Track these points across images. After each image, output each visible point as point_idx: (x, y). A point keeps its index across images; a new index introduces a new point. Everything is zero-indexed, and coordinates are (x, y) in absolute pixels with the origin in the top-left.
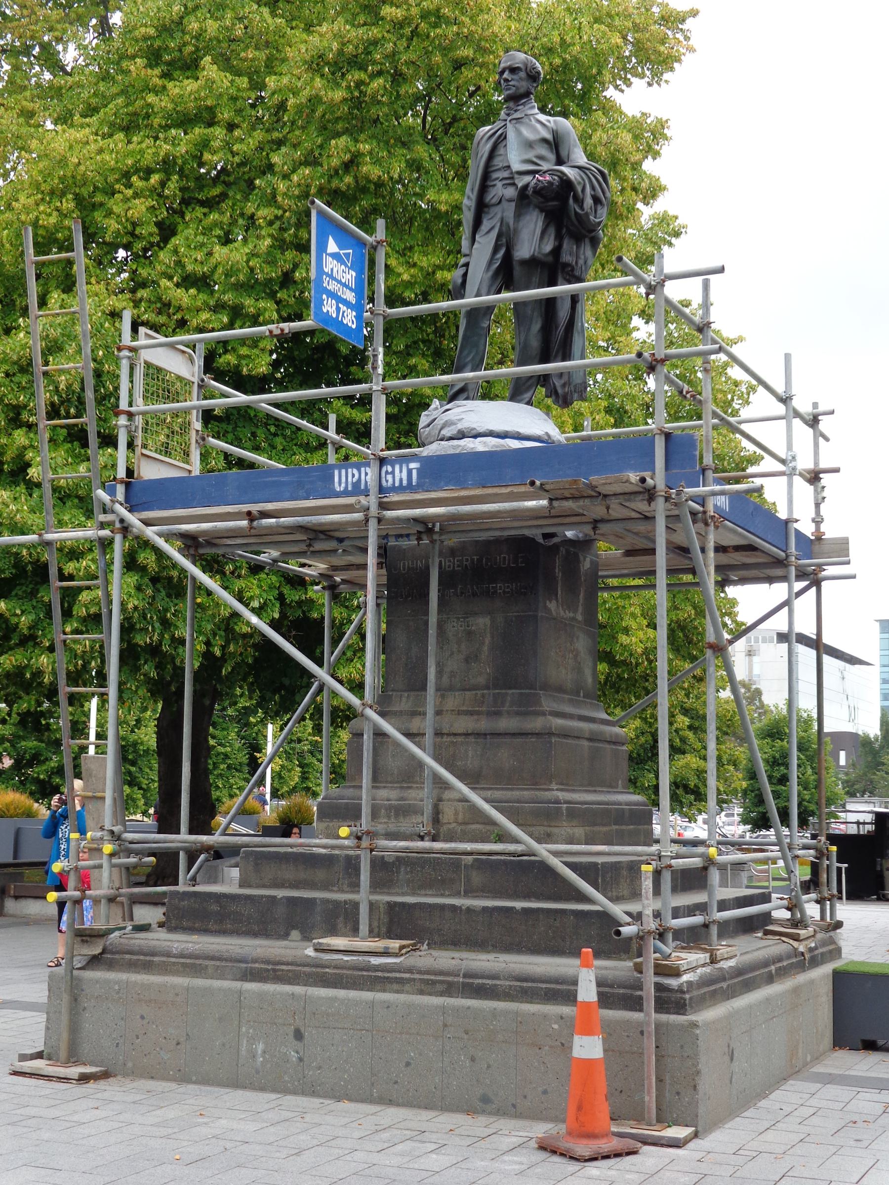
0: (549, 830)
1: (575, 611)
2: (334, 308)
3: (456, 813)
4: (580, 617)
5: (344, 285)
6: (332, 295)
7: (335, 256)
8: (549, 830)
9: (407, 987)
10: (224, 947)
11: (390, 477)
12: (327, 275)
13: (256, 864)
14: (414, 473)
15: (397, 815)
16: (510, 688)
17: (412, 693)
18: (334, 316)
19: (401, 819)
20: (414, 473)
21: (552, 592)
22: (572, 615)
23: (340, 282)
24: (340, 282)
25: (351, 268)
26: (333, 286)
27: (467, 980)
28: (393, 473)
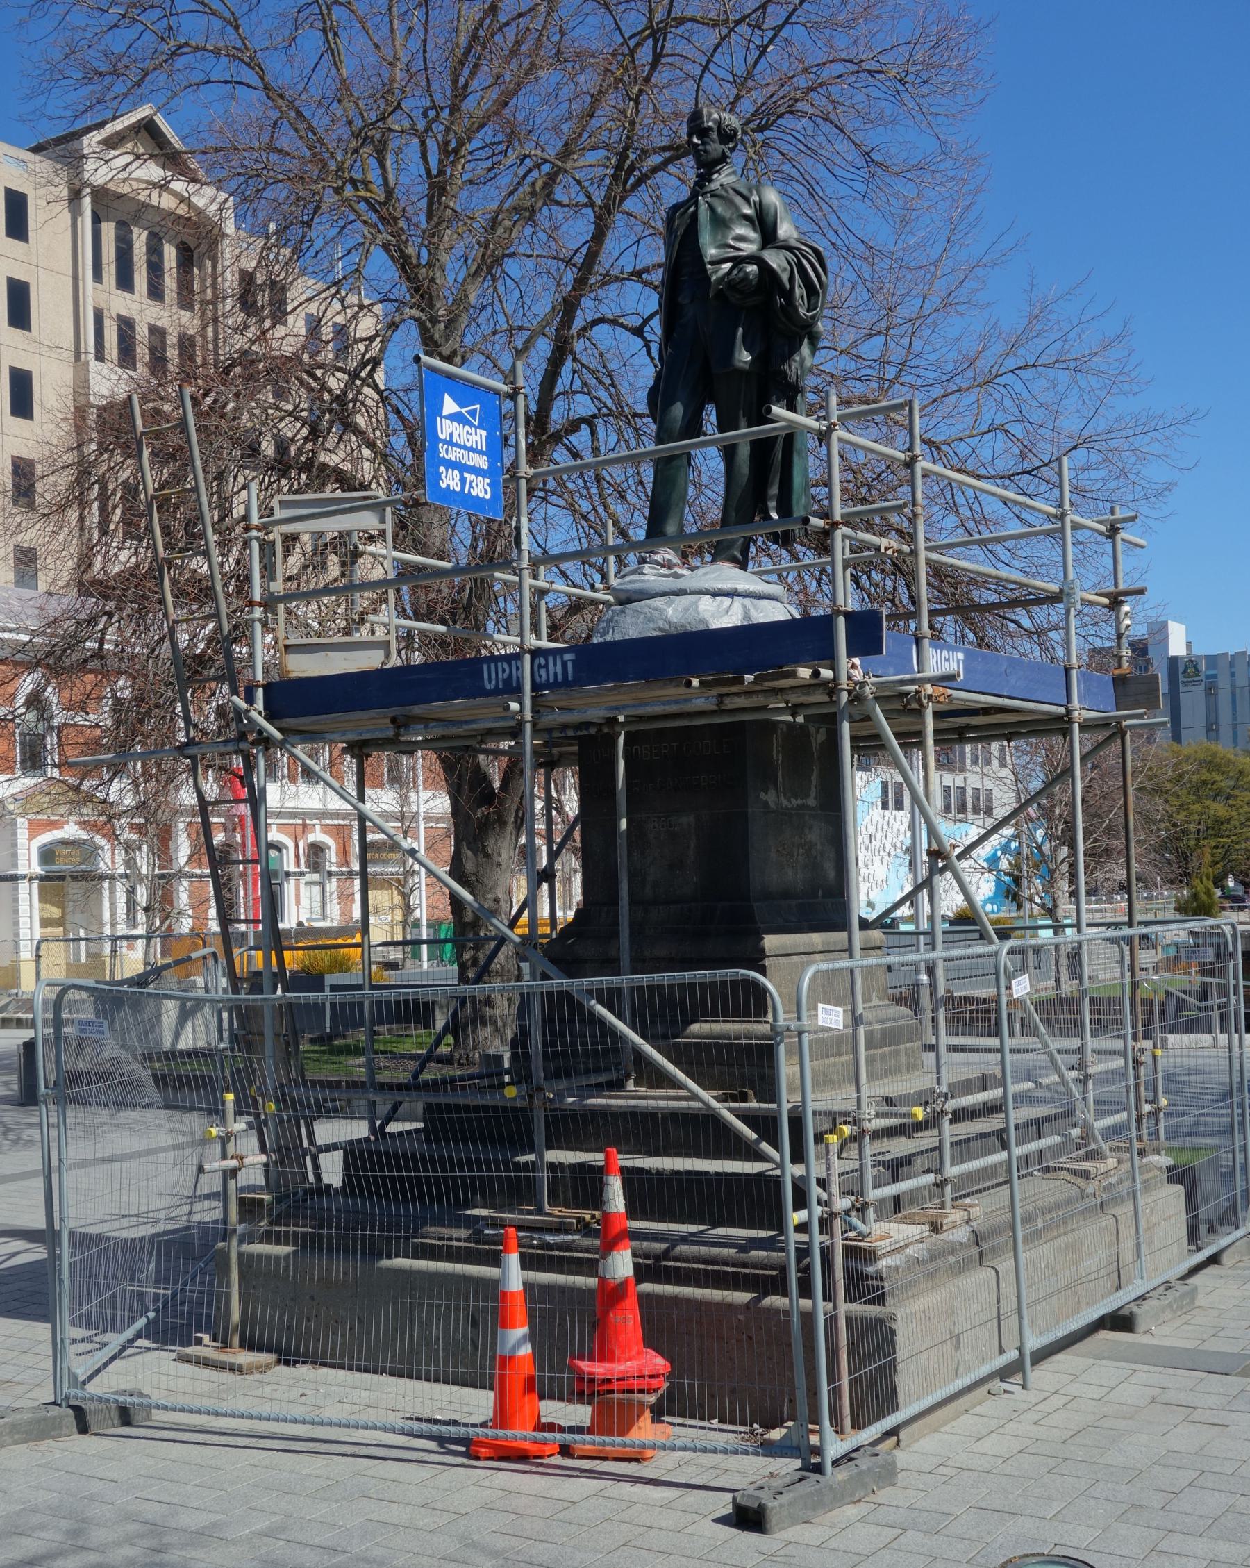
1: (807, 796)
2: (457, 479)
4: (811, 802)
5: (471, 449)
6: (452, 465)
7: (454, 417)
11: (543, 672)
12: (445, 442)
14: (570, 665)
18: (458, 489)
20: (570, 665)
21: (768, 778)
22: (800, 802)
23: (464, 447)
24: (464, 447)
25: (480, 426)
26: (453, 454)
28: (546, 666)
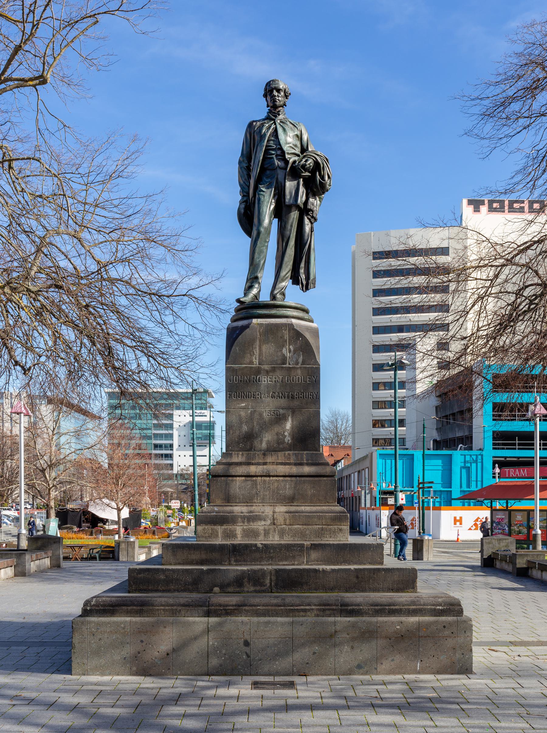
0: (340, 527)
3: (285, 520)
8: (340, 527)
9: (309, 613)
10: (109, 599)
13: (174, 551)
15: (249, 521)
16: (304, 451)
17: (245, 453)
19: (252, 524)
27: (343, 608)
